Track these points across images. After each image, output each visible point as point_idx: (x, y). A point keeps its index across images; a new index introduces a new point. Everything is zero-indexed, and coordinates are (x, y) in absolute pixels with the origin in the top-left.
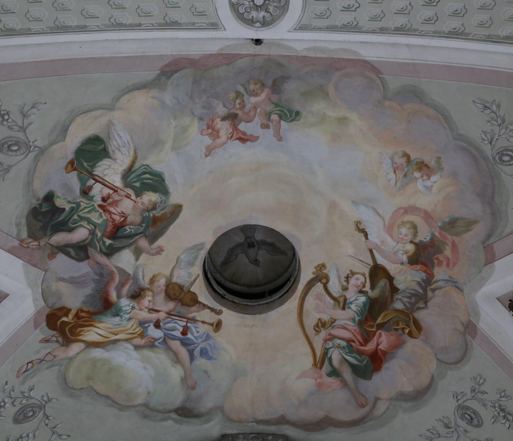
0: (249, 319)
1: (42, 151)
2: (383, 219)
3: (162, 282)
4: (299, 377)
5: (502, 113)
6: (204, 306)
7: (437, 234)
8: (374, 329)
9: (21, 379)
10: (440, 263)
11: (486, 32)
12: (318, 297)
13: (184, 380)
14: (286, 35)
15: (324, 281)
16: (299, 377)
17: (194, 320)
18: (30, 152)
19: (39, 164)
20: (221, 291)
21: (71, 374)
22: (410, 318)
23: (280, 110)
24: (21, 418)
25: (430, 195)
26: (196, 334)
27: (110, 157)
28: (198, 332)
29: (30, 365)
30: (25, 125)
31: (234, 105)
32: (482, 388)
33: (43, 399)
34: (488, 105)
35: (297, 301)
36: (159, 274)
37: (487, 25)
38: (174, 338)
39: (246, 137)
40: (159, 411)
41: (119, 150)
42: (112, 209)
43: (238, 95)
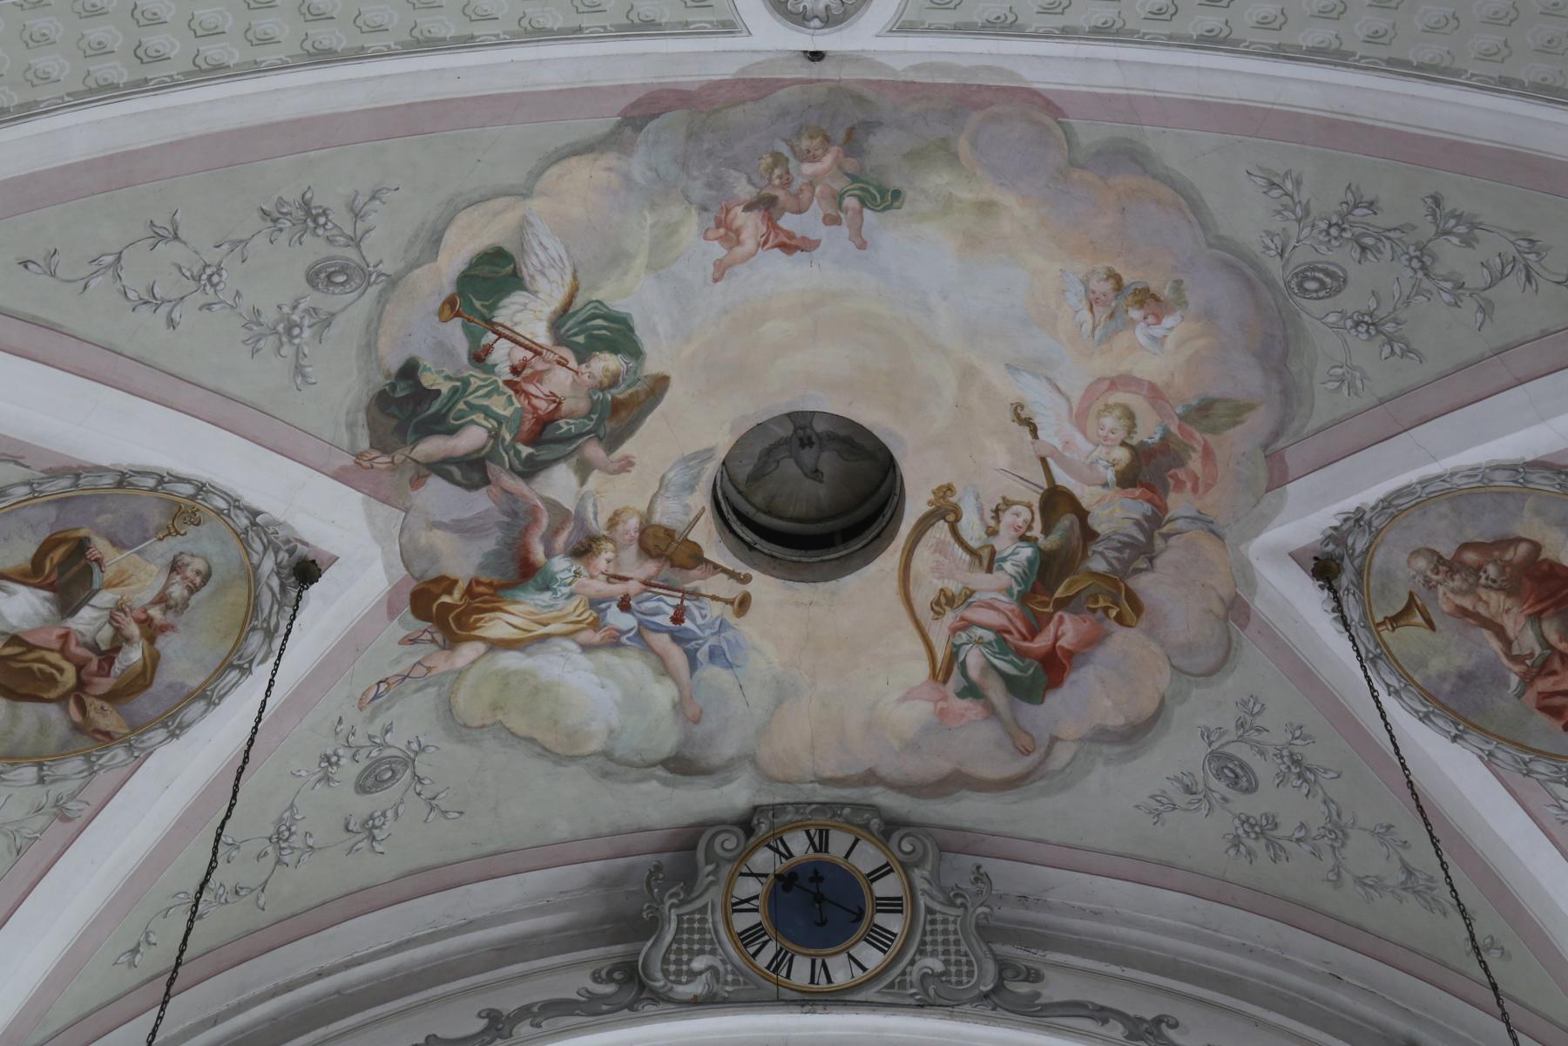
0: (804, 591)
1: (393, 282)
2: (1068, 400)
3: (633, 523)
4: (904, 699)
5: (1304, 196)
6: (716, 567)
7: (1174, 429)
8: (1049, 609)
9: (367, 712)
10: (1180, 485)
11: (1274, 38)
12: (940, 548)
13: (678, 707)
14: (871, 42)
15: (951, 518)
16: (904, 699)
17: (696, 595)
18: (369, 284)
19: (388, 307)
20: (749, 536)
21: (462, 701)
22: (1119, 589)
23: (861, 189)
24: (370, 782)
25: (1161, 353)
26: (700, 621)
27: (524, 288)
28: (704, 617)
29: (383, 687)
30: (359, 233)
31: (770, 180)
32: (1258, 722)
33: (409, 748)
34: (1276, 180)
35: (898, 554)
36: (625, 509)
37: (1276, 25)
38: (659, 629)
39: (793, 243)
40: (631, 765)
41: (544, 274)
42: (531, 389)
43: (778, 159)
